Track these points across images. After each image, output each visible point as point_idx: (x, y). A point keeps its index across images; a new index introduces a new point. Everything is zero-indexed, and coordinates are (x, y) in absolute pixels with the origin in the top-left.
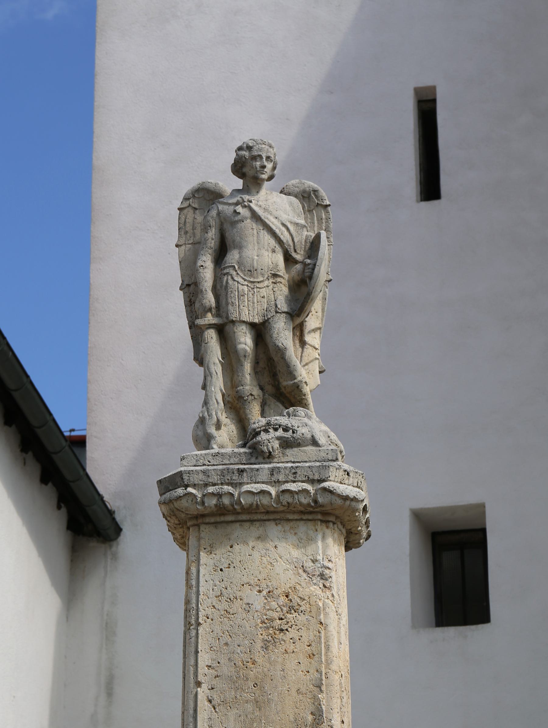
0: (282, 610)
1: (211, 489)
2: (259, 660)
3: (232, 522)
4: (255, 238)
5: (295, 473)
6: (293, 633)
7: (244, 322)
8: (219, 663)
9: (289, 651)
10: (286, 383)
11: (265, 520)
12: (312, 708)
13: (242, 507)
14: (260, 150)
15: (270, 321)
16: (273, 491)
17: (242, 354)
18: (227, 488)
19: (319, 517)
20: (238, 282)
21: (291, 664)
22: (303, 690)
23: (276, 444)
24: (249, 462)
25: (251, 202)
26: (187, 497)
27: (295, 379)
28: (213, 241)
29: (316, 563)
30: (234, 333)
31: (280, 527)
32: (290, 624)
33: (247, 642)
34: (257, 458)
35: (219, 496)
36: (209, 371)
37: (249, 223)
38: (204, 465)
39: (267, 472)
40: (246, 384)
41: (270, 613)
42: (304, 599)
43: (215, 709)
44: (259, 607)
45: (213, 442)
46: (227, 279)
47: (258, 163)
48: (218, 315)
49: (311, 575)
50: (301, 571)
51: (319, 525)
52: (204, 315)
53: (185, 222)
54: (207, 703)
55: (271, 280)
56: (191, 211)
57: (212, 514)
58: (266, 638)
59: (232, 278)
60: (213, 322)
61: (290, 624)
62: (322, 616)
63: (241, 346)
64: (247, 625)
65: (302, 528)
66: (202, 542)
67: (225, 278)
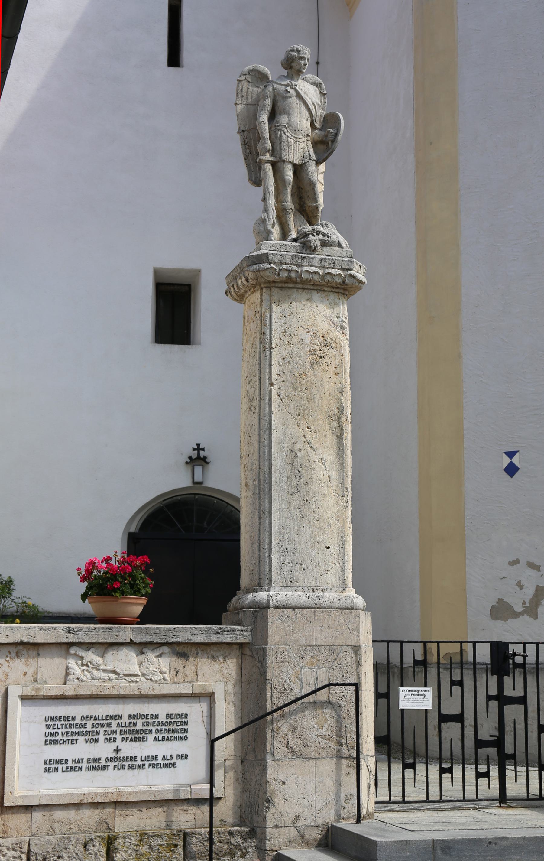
0: (321, 345)
1: (285, 267)
2: (309, 374)
3: (292, 288)
4: (298, 110)
5: (334, 263)
6: (327, 359)
7: (290, 162)
8: (284, 373)
9: (325, 370)
10: (310, 204)
11: (311, 289)
12: (338, 405)
13: (301, 280)
14: (305, 54)
15: (307, 164)
16: (321, 272)
17: (287, 182)
18: (294, 267)
19: (342, 291)
20: (288, 136)
21: (326, 378)
22: (333, 393)
23: (318, 243)
24: (301, 252)
25: (296, 86)
26: (270, 270)
27: (317, 202)
28: (269, 107)
29: (339, 319)
30: (284, 168)
31: (319, 294)
32: (325, 354)
33: (301, 362)
34: (306, 250)
35: (289, 271)
36: (268, 191)
37: (294, 100)
38: (275, 250)
39: (318, 260)
40: (288, 201)
41: (314, 346)
42: (333, 340)
43: (281, 400)
44: (308, 342)
45: (271, 235)
46: (281, 134)
47: (302, 62)
48: (273, 155)
49: (336, 326)
50: (331, 322)
51: (341, 297)
52: (264, 154)
53: (242, 89)
54: (277, 397)
55: (306, 138)
56: (246, 83)
57: (281, 282)
58: (312, 361)
59: (284, 133)
60: (271, 159)
61: (325, 354)
62: (343, 351)
63: (287, 178)
64: (301, 352)
65: (332, 296)
66: (273, 298)
67: (279, 132)
